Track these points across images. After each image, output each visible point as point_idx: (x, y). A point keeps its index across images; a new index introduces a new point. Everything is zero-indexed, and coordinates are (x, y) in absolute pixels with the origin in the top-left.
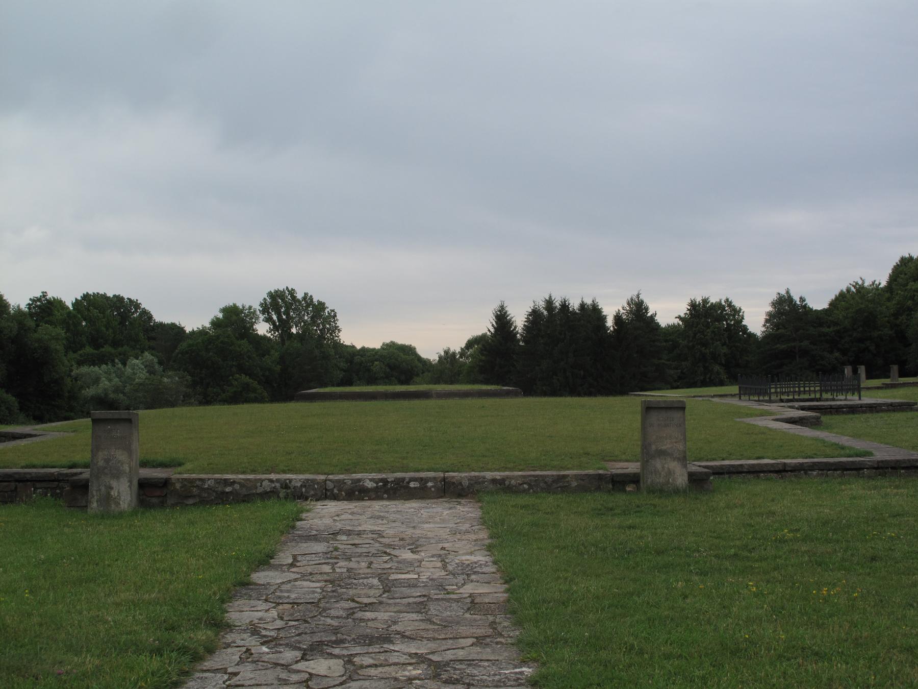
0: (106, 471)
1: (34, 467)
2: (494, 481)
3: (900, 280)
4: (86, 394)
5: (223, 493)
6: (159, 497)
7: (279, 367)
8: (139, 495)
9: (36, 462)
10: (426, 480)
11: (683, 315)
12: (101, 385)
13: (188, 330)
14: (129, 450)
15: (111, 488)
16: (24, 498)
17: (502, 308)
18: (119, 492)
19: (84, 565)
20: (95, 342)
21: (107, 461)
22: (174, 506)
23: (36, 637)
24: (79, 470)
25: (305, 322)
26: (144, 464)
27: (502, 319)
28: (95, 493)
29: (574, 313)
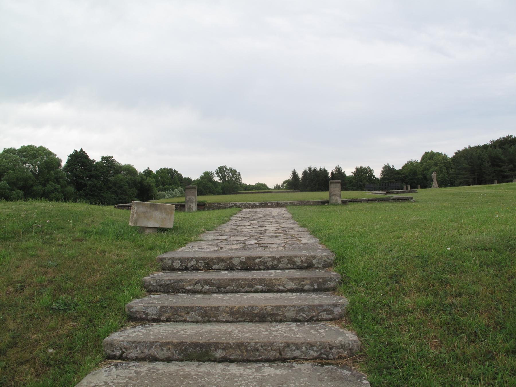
2: (290, 203)
3: (424, 159)
5: (219, 207)
7: (222, 190)
8: (198, 208)
10: (273, 203)
11: (354, 172)
13: (193, 180)
17: (294, 170)
20: (163, 184)
22: (207, 210)
25: (230, 176)
27: (295, 174)
29: (318, 171)
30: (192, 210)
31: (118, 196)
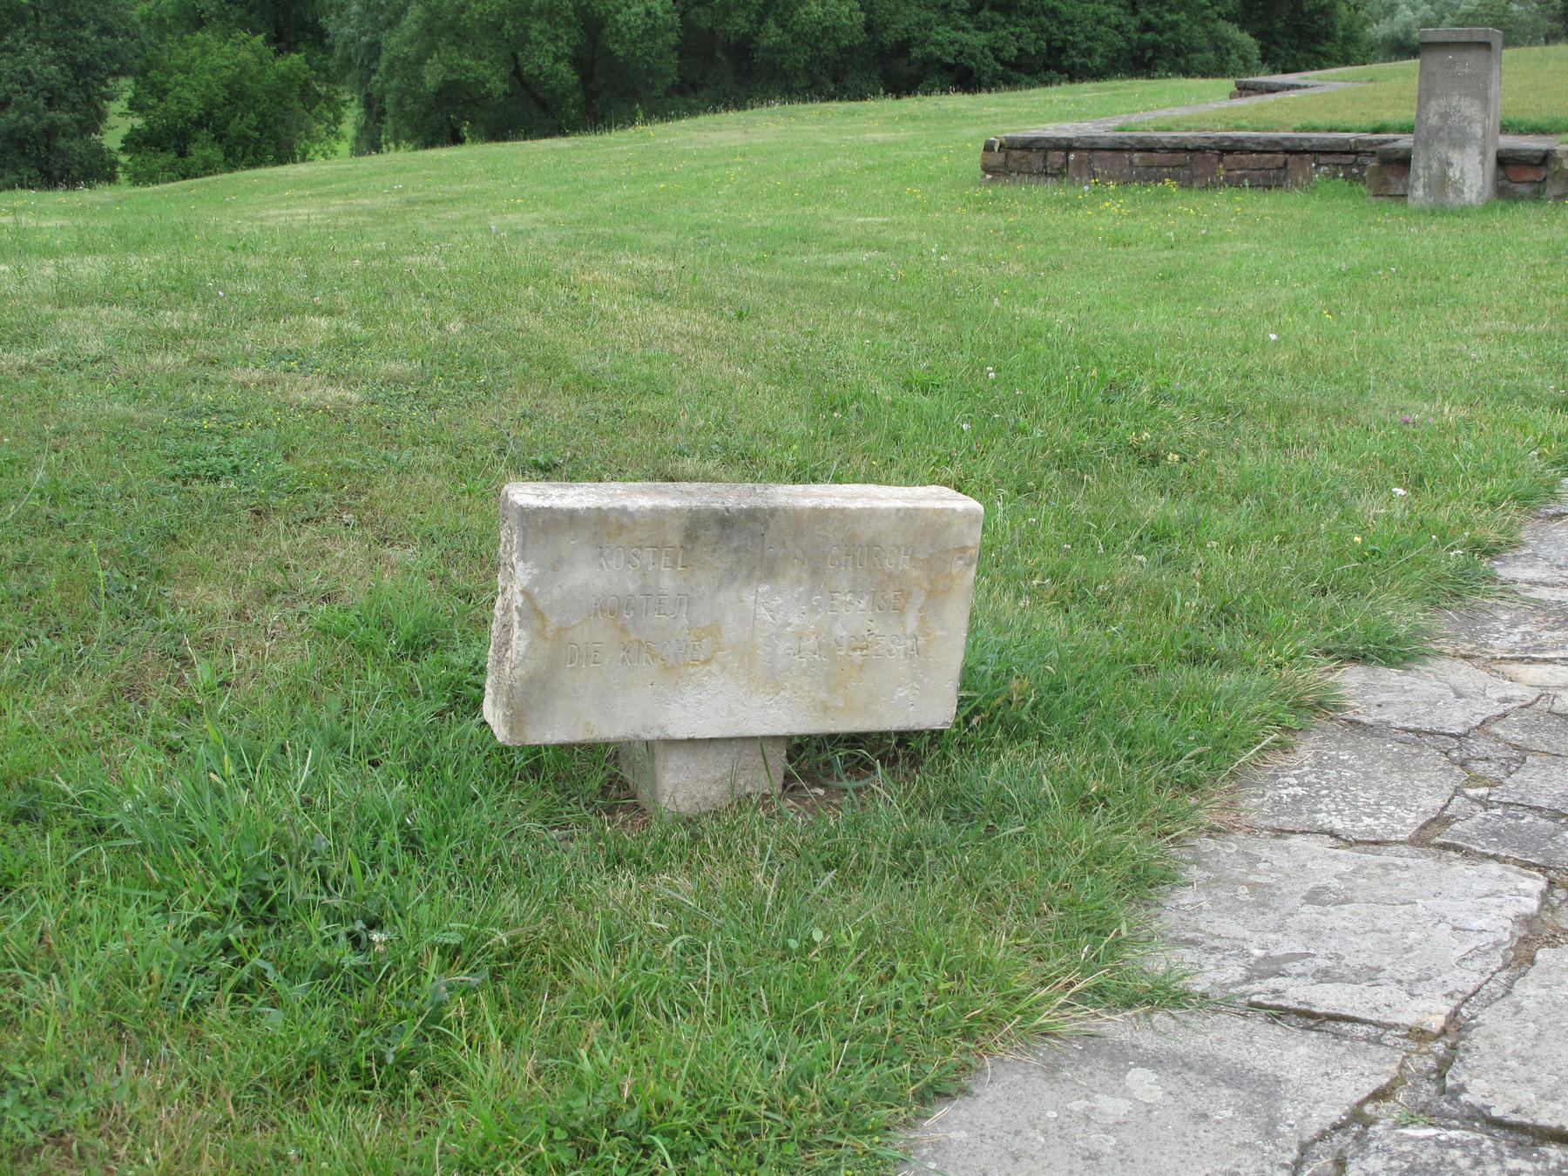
0: (1441, 134)
1: (1315, 129)
4: (1373, 33)
6: (1532, 182)
8: (1497, 179)
9: (1317, 122)
12: (1399, 18)
14: (1484, 99)
15: (1450, 165)
16: (1300, 178)
18: (1462, 172)
19: (1414, 280)
21: (1444, 116)
23: (1357, 371)
24: (1391, 136)
26: (1505, 129)
28: (1420, 172)
30: (1460, 192)
31: (1135, 12)
